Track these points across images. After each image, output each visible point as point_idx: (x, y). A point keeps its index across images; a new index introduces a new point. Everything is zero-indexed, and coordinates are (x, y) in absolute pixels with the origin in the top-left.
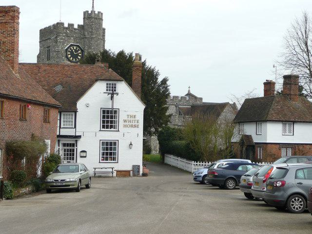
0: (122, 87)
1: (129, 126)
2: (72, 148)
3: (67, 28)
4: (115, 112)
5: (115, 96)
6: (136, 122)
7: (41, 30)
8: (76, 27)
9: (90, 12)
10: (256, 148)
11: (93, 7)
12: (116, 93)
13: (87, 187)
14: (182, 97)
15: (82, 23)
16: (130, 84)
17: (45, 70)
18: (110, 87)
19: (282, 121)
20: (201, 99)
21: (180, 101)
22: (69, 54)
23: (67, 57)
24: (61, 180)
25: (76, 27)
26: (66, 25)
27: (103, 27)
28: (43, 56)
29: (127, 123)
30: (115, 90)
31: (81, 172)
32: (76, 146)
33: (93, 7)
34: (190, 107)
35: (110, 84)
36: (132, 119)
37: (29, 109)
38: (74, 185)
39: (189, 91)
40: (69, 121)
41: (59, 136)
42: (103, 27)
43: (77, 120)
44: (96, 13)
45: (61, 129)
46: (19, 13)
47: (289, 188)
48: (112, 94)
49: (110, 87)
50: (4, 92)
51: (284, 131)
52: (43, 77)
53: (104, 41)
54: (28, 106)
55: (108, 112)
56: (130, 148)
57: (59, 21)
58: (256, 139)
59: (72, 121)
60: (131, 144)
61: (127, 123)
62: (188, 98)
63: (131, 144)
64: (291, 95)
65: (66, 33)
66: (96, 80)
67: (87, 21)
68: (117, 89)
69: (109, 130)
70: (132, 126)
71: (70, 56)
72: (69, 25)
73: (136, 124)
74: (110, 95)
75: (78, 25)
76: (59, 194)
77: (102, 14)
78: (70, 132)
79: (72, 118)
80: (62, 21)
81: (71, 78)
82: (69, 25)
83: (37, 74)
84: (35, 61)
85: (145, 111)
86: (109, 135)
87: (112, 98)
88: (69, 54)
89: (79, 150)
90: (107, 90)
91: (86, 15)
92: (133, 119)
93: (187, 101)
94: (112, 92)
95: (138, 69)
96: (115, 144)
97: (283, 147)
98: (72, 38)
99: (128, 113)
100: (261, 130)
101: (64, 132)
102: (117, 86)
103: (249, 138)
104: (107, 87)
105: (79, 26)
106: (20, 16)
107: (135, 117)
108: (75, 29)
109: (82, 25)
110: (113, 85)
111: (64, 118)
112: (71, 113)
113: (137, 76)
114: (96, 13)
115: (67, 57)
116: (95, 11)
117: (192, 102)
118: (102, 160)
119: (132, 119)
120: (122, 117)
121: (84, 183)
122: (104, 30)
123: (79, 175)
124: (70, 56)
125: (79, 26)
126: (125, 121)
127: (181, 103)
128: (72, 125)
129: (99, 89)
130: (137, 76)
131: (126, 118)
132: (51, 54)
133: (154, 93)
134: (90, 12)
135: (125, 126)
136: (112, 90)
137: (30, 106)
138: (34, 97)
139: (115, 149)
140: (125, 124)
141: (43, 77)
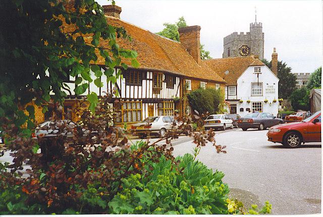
5: (259, 74)
7: (224, 38)
15: (249, 31)
25: (245, 34)
26: (239, 34)
36: (271, 88)
44: (258, 23)
50: (191, 76)
53: (263, 41)
70: (271, 92)
72: (241, 33)
76: (289, 149)
82: (241, 33)
101: (230, 98)
105: (247, 33)
114: (258, 23)
120: (265, 86)
125: (247, 33)
126: (266, 90)
133: (74, 102)
135: (266, 93)
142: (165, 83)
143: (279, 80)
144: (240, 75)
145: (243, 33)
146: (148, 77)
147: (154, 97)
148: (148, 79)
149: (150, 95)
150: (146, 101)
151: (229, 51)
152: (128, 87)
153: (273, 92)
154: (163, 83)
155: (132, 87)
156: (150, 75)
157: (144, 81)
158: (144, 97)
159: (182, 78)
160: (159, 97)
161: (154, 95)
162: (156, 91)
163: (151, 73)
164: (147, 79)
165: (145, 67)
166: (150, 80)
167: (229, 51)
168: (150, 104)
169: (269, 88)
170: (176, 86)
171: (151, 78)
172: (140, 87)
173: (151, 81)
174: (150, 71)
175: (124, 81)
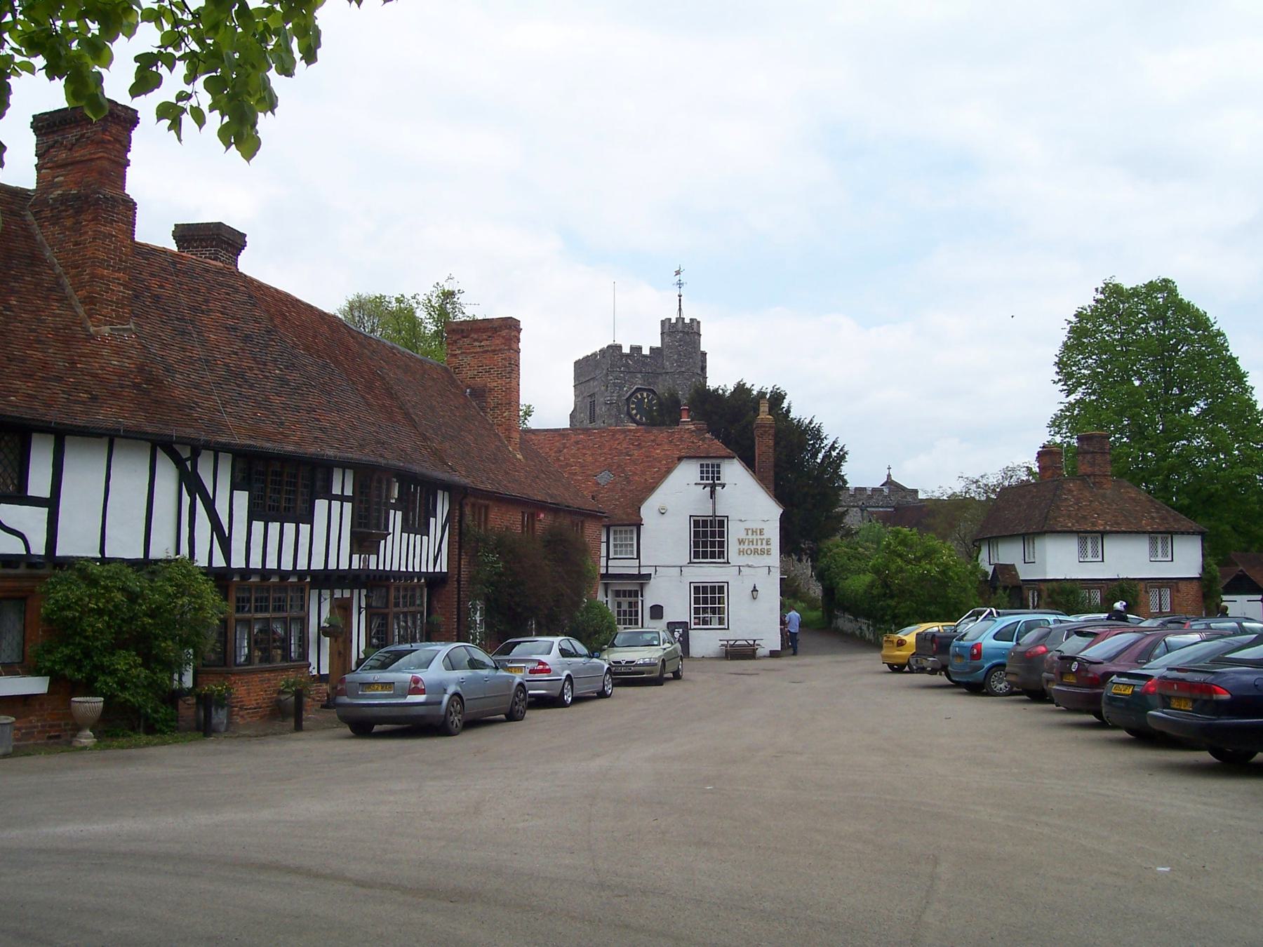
0: (734, 473)
1: (749, 552)
2: (632, 599)
3: (627, 355)
4: (721, 524)
6: (764, 542)
8: (646, 351)
9: (673, 321)
10: (1025, 592)
11: (680, 309)
12: (720, 484)
13: (677, 676)
14: (874, 490)
16: (749, 463)
17: (577, 443)
18: (708, 472)
19: (1077, 532)
20: (916, 492)
21: (870, 497)
22: (633, 409)
23: (629, 414)
24: (627, 662)
25: (646, 351)
26: (626, 350)
27: (702, 349)
28: (582, 415)
29: (746, 547)
30: (718, 479)
31: (664, 647)
32: (642, 596)
33: (680, 309)
34: (892, 510)
35: (708, 466)
36: (755, 537)
37: (540, 520)
38: (651, 672)
39: (889, 476)
40: (626, 545)
41: (606, 576)
42: (702, 349)
43: (210, 539)
44: (687, 321)
45: (610, 561)
46: (519, 330)
47: (216, 710)
48: (713, 487)
49: (708, 472)
50: (489, 487)
51: (1153, 552)
52: (574, 456)
54: (538, 516)
55: (705, 522)
56: (755, 598)
57: (611, 342)
58: (1025, 573)
59: (633, 544)
60: (755, 590)
62: (886, 490)
63: (755, 590)
64: (1095, 475)
65: (627, 366)
66: (680, 459)
67: (667, 339)
68: (721, 476)
70: (756, 552)
71: (634, 412)
72: (632, 348)
74: (708, 489)
75: (651, 348)
77: (699, 323)
78: (629, 567)
79: (632, 539)
81: (629, 455)
82: (632, 348)
83: (561, 451)
84: (566, 424)
85: (784, 520)
86: (709, 573)
87: (713, 493)
88: (633, 409)
89: (649, 603)
90: (702, 478)
91: (667, 324)
92: (759, 537)
93: (886, 497)
94: (712, 481)
95: (765, 432)
96: (721, 589)
97: (1151, 587)
98: (639, 376)
99: (748, 525)
100: (998, 555)
102: (722, 469)
103: (1010, 569)
104: (702, 472)
105: (651, 349)
106: (522, 335)
108: (645, 356)
109: (657, 348)
111: (615, 539)
112: (631, 528)
113: (764, 447)
114: (687, 321)
115: (629, 414)
116: (684, 319)
117: (894, 500)
118: (695, 624)
120: (734, 532)
121: (670, 667)
122: (704, 354)
123: (661, 653)
124: (634, 412)
125: (651, 349)
126: (741, 542)
127: (872, 502)
128: (632, 553)
129: (686, 476)
130: (764, 447)
131: (743, 535)
132: (597, 409)
134: (673, 321)
135: (741, 552)
136: (713, 479)
137: (542, 516)
138: (551, 496)
139: (721, 601)
141: (574, 456)
142: (399, 514)
143: (781, 511)
144: (651, 489)
145: (640, 348)
146: (336, 490)
147: (355, 566)
148: (336, 498)
149: (344, 559)
150: (326, 579)
151: (593, 405)
152: (258, 526)
153: (762, 552)
154: (392, 512)
155: (274, 527)
156: (342, 484)
157: (321, 505)
158: (318, 564)
159: (459, 494)
160: (373, 566)
161: (356, 557)
162: (365, 539)
163: (1167, 593)
164: (331, 498)
165: (331, 453)
166: (342, 498)
167: (593, 405)
168: (338, 594)
169: (750, 537)
170: (436, 524)
171: (349, 492)
172: (304, 528)
173: (348, 507)
174: (345, 465)
175: (242, 498)
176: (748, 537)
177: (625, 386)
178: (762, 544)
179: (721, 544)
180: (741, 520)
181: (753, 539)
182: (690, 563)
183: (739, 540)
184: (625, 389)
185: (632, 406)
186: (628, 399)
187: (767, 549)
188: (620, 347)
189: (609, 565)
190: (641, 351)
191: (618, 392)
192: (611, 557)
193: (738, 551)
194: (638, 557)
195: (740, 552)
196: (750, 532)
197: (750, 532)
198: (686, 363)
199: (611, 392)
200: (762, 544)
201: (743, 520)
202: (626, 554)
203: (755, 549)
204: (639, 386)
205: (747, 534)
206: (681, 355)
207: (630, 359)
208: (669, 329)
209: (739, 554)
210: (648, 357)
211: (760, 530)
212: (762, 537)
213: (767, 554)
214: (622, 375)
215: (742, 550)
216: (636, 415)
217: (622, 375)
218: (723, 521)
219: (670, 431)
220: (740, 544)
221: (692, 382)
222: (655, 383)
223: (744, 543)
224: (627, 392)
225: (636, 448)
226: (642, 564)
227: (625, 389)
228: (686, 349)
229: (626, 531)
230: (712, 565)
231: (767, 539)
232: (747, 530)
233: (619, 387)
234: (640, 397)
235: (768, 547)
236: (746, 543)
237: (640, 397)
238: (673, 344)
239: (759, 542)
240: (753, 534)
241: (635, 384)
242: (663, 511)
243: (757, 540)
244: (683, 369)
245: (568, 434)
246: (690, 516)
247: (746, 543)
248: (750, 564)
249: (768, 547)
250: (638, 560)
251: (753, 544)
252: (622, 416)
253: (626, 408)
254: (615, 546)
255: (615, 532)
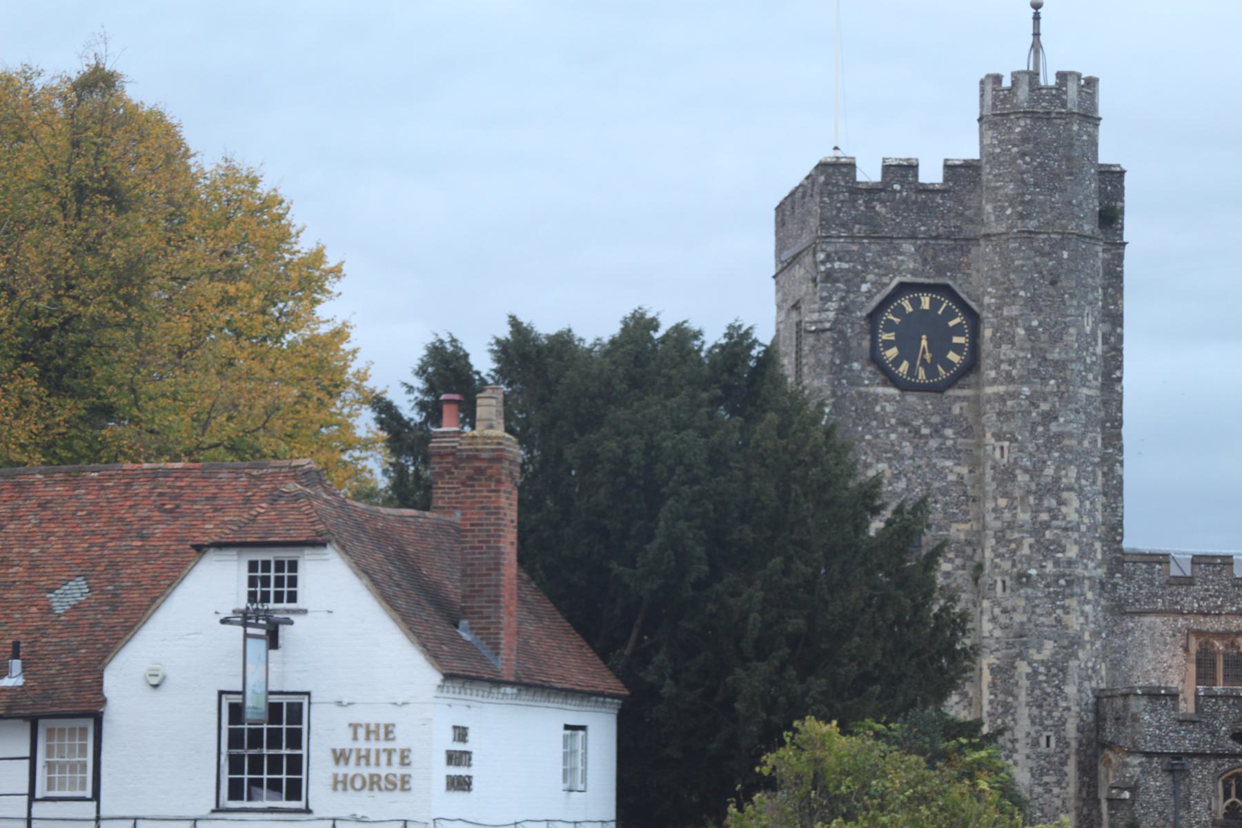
1: (358, 784)
3: (871, 191)
6: (396, 758)
8: (931, 174)
15: (968, 148)
22: (888, 344)
23: (875, 359)
25: (931, 174)
26: (869, 173)
27: (1105, 157)
29: (351, 770)
36: (373, 745)
49: (266, 582)
57: (827, 154)
59: (84, 766)
61: (351, 770)
65: (870, 220)
66: (200, 549)
68: (301, 589)
69: (245, 804)
70: (373, 783)
71: (892, 353)
73: (397, 770)
80: (846, 153)
82: (887, 169)
88: (888, 344)
92: (383, 745)
95: (480, 471)
98: (908, 247)
105: (950, 169)
107: (389, 731)
110: (280, 566)
111: (49, 752)
112: (78, 723)
115: (875, 359)
119: (373, 745)
122: (1113, 178)
124: (892, 353)
125: (950, 169)
126: (340, 757)
135: (342, 784)
140: (342, 770)
169: (362, 744)
176: (356, 745)
177: (864, 281)
178: (389, 763)
179: (296, 764)
180: (340, 703)
181: (368, 751)
182: (218, 809)
183: (334, 751)
184: (864, 288)
185: (885, 337)
186: (873, 317)
187: (403, 777)
188: (851, 166)
189: (34, 815)
190: (916, 176)
191: (843, 299)
192: (38, 795)
193: (331, 781)
194: (96, 796)
195: (336, 783)
196: (362, 732)
197: (362, 732)
198: (1041, 204)
199: (822, 299)
200: (389, 763)
201: (345, 701)
202: (72, 787)
203: (372, 776)
204: (909, 278)
205: (355, 738)
206: (1024, 182)
207: (882, 202)
208: (994, 106)
209: (335, 789)
210: (938, 191)
211: (387, 726)
212: (389, 745)
213: (403, 789)
214: (855, 248)
215: (340, 778)
216: (897, 362)
217: (855, 248)
218: (300, 705)
219: (255, 473)
220: (337, 761)
221: (1060, 261)
222: (956, 268)
223: (347, 761)
224: (870, 295)
225: (166, 517)
226: (103, 813)
227: (864, 288)
228: (1040, 164)
229: (72, 730)
230: (275, 816)
231: (403, 751)
232: (355, 727)
233: (847, 282)
234: (909, 309)
235: (405, 771)
236: (353, 759)
237: (909, 309)
238: (1005, 152)
239: (384, 758)
240: (368, 738)
241: (897, 271)
242: (155, 681)
243: (378, 752)
244: (1032, 224)
245: (32, 484)
246: (221, 693)
247: (353, 759)
248: (359, 814)
249: (405, 771)
250: (95, 803)
251: (368, 764)
252: (856, 366)
253: (866, 344)
254: (50, 766)
255: (50, 732)
